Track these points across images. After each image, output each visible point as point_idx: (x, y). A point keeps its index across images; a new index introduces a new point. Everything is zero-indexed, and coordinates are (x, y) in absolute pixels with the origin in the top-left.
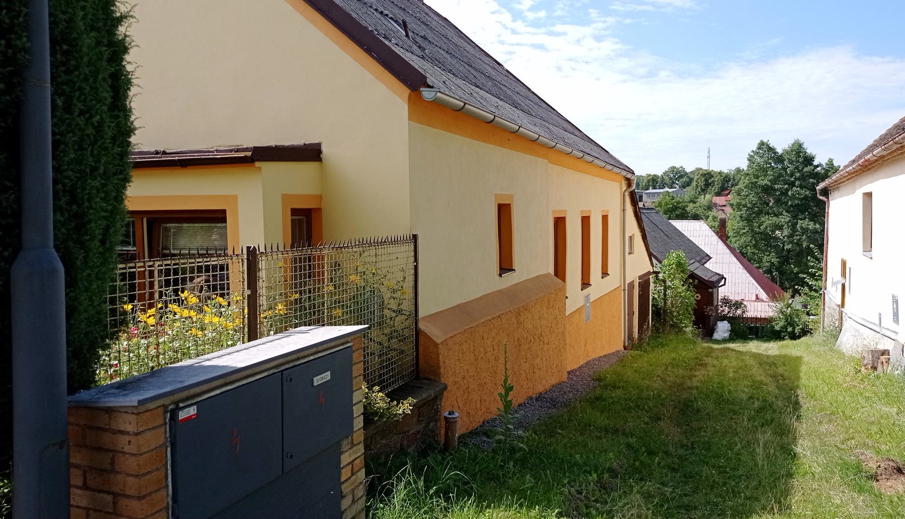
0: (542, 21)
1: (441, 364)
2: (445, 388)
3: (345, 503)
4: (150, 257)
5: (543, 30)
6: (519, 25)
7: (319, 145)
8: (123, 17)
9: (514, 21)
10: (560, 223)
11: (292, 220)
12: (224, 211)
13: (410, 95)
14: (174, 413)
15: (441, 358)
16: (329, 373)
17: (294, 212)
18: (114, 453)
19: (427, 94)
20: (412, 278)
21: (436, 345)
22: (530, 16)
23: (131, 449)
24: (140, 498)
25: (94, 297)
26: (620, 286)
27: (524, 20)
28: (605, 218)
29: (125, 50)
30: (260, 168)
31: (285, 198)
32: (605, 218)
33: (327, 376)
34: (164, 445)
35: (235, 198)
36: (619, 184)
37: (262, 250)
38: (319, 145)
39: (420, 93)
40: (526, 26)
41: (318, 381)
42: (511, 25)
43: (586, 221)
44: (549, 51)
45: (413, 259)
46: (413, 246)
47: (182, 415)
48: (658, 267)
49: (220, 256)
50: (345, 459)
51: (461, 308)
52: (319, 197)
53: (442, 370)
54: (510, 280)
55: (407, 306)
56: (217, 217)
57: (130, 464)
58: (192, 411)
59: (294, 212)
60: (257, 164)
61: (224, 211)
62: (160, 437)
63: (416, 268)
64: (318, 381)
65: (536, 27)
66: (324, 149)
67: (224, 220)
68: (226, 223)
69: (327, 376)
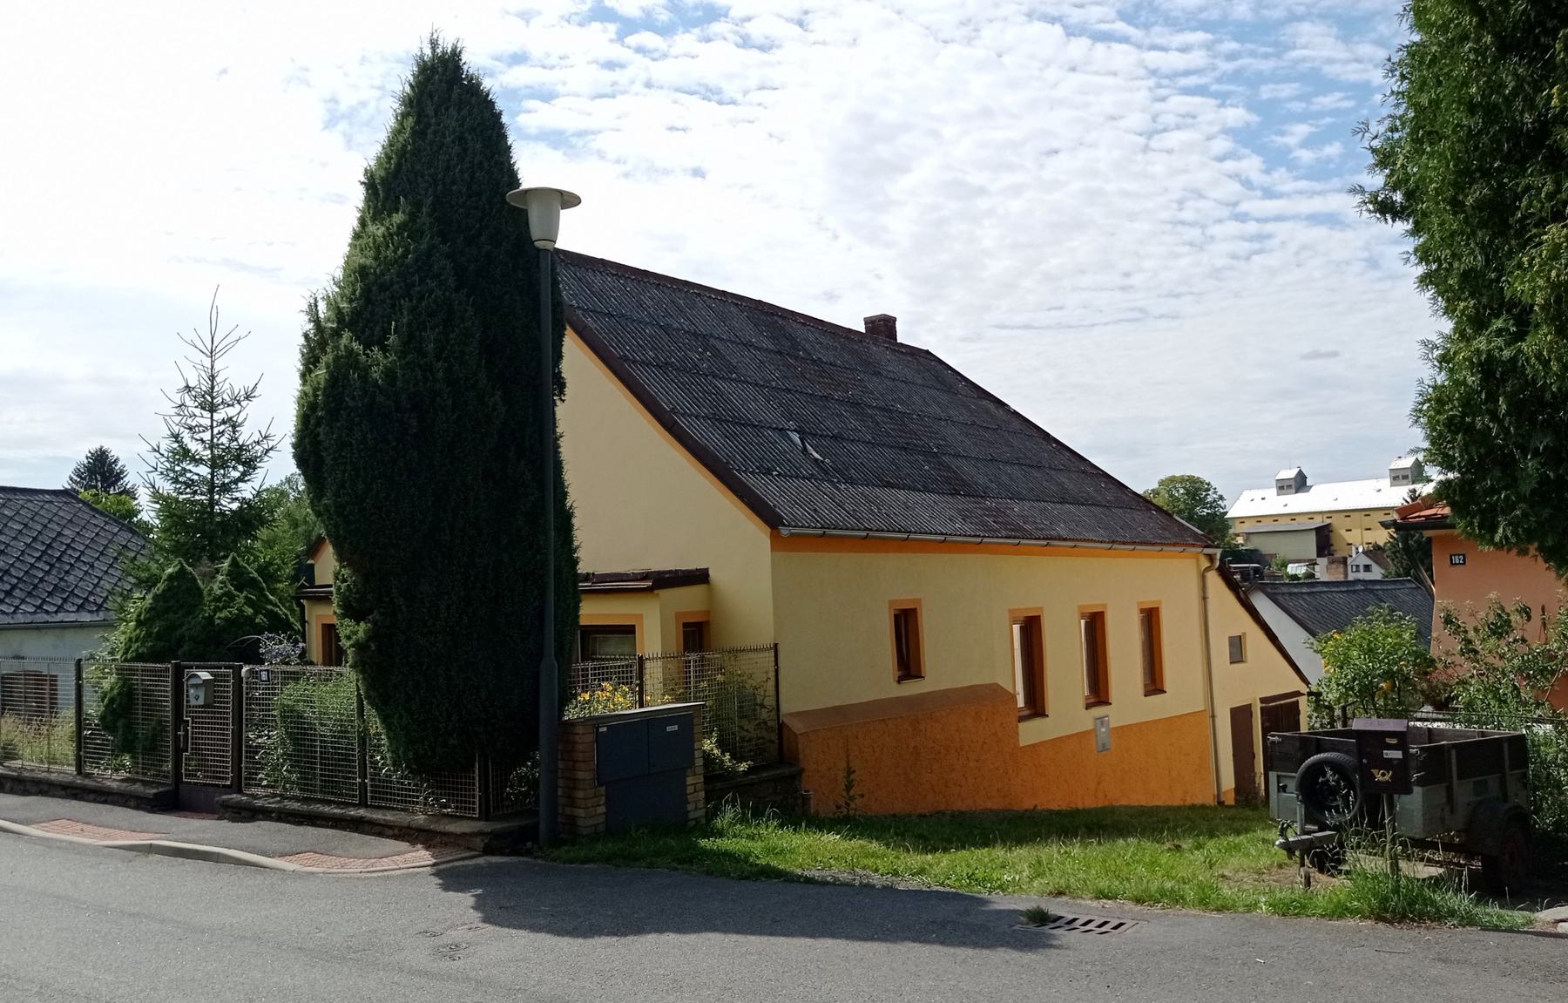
0: (1332, 166)
1: (800, 751)
2: (802, 771)
3: (690, 807)
4: (582, 661)
5: (1336, 183)
6: (1281, 179)
7: (707, 570)
8: (578, 547)
9: (1267, 172)
10: (1031, 628)
11: (684, 632)
12: (634, 626)
13: (771, 534)
14: (598, 730)
15: (800, 746)
16: (676, 726)
17: (685, 625)
18: (575, 742)
19: (784, 531)
20: (773, 679)
21: (796, 735)
22: (1306, 156)
23: (580, 741)
24: (584, 761)
25: (1489, 61)
26: (1205, 711)
27: (1292, 165)
28: (1151, 618)
29: (578, 563)
30: (658, 594)
31: (678, 615)
32: (1151, 618)
33: (676, 728)
34: (593, 742)
35: (641, 616)
36: (1195, 560)
37: (647, 657)
38: (707, 570)
39: (779, 531)
40: (1297, 178)
41: (669, 729)
42: (1256, 177)
43: (1095, 624)
44: (1348, 226)
45: (773, 664)
46: (773, 654)
47: (601, 730)
48: (1324, 686)
49: (621, 659)
50: (690, 780)
51: (839, 711)
52: (708, 612)
53: (801, 756)
54: (912, 688)
55: (770, 702)
56: (629, 630)
57: (580, 747)
58: (605, 729)
59: (685, 625)
60: (656, 592)
61: (634, 626)
62: (591, 738)
63: (777, 671)
64: (669, 729)
65: (1318, 180)
66: (711, 573)
67: (634, 633)
68: (635, 633)
69: (676, 728)
